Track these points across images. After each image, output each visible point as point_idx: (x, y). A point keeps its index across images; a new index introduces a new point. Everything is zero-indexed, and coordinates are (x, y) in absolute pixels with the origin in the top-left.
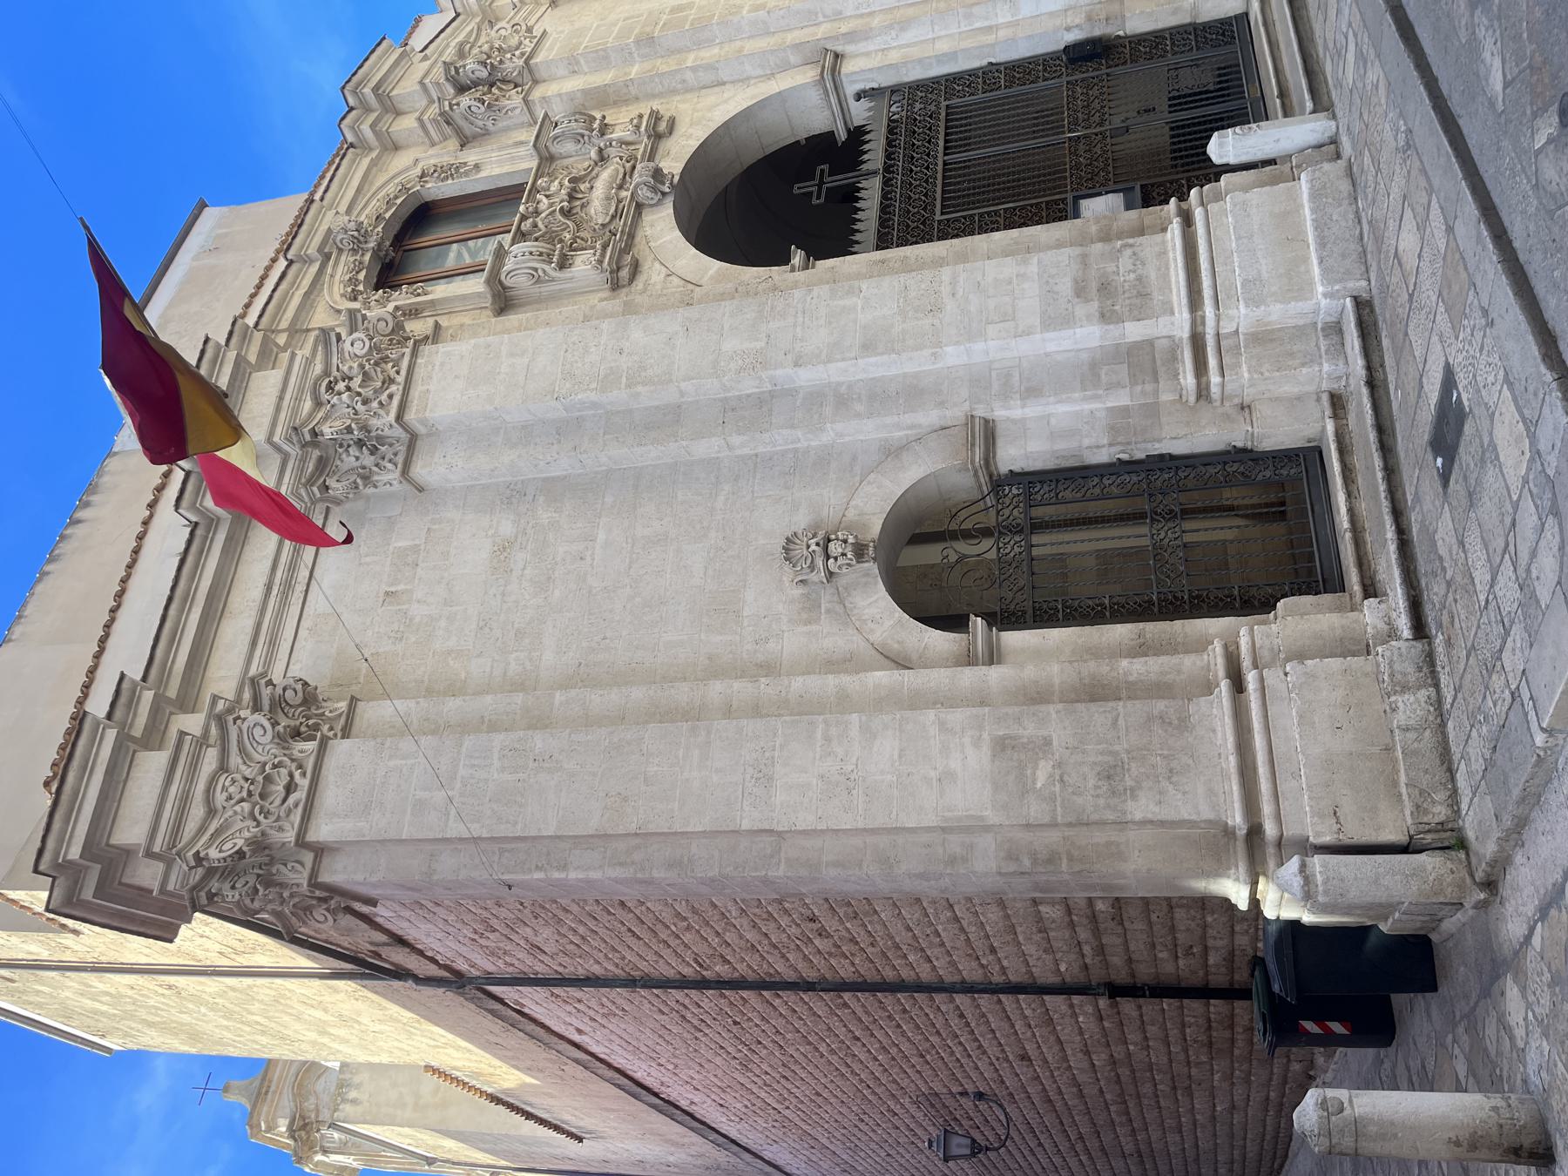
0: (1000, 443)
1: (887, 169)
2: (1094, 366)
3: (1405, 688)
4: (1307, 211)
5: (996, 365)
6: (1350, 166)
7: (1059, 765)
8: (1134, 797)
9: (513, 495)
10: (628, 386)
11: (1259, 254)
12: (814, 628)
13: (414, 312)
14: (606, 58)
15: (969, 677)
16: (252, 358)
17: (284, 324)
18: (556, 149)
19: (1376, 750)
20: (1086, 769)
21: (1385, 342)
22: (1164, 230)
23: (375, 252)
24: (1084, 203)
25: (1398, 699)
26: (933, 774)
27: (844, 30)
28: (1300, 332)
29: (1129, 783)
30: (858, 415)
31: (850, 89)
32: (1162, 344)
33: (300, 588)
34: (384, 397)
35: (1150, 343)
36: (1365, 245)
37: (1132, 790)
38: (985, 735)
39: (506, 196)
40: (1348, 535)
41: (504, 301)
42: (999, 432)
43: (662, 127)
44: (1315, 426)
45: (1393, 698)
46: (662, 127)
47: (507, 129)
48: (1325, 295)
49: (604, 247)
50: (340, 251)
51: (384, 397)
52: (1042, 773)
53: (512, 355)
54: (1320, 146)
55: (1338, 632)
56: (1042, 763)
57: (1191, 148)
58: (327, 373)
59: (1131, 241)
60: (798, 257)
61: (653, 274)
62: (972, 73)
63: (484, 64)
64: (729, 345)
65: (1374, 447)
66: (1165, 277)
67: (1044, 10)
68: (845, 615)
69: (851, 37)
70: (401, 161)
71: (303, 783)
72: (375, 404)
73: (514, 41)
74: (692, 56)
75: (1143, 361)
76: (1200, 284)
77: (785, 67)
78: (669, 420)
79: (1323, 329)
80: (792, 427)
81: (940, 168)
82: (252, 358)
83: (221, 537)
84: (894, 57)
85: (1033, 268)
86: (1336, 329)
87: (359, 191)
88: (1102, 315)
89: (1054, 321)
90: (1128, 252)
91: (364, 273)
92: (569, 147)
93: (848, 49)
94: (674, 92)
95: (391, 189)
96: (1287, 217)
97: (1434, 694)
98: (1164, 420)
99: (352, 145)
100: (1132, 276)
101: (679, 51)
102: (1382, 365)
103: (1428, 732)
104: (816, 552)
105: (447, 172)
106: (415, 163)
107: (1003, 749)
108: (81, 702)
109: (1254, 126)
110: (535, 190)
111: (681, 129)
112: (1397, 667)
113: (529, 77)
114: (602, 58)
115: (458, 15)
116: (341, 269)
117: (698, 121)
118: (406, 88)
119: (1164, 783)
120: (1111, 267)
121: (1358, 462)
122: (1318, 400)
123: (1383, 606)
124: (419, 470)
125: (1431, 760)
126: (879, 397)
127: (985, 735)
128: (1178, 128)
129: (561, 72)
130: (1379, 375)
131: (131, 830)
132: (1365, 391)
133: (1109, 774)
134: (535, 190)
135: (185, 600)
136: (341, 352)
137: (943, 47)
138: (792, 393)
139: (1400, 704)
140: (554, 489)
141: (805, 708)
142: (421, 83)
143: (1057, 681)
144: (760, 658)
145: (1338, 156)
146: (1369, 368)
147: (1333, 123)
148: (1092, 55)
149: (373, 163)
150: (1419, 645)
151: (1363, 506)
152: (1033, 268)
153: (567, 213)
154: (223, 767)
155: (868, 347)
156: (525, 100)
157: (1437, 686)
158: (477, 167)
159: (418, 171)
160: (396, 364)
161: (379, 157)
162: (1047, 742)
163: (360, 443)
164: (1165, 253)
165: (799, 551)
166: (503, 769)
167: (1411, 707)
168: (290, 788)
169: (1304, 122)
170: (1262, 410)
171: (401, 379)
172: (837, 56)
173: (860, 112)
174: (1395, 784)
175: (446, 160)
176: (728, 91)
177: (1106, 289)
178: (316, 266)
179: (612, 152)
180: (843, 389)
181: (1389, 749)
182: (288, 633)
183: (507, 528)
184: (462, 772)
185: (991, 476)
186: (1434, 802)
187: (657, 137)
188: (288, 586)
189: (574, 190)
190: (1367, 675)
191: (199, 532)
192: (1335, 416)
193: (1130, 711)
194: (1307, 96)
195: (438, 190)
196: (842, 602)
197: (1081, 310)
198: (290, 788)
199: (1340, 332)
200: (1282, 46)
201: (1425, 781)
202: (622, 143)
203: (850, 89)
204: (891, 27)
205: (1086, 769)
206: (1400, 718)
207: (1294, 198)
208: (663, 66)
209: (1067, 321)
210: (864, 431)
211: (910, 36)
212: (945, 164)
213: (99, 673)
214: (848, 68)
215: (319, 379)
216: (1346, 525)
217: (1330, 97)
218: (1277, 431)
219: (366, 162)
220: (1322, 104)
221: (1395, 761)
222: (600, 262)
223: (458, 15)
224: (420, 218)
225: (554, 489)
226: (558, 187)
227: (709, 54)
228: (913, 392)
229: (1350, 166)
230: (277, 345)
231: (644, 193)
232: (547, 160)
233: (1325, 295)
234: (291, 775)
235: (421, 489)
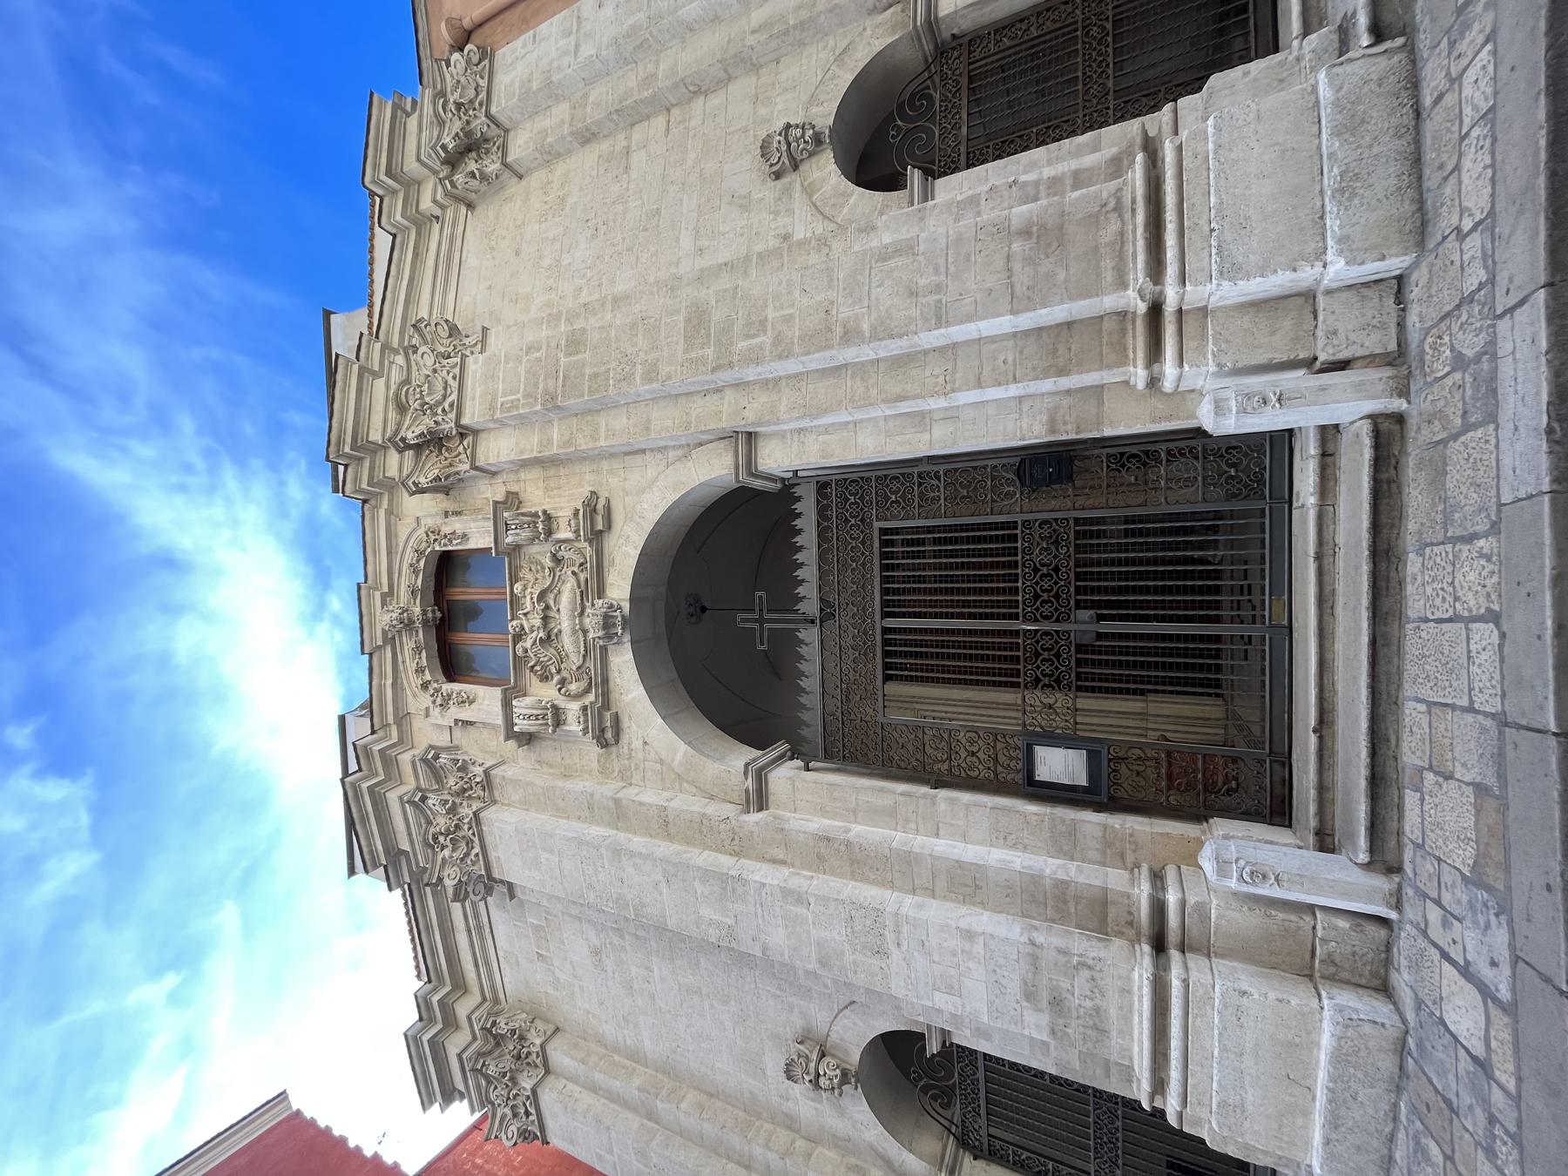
11: (1247, 1079)
33: (487, 930)
50: (399, 632)
66: (1127, 1020)
68: (842, 1113)
76: (1167, 1048)
87: (389, 553)
91: (424, 654)
95: (410, 556)
104: (810, 1060)
115: (394, 236)
120: (1065, 984)
135: (427, 929)
182: (493, 957)
185: (944, 1042)
187: (597, 537)
188: (480, 928)
198: (527, 1114)
223: (394, 236)
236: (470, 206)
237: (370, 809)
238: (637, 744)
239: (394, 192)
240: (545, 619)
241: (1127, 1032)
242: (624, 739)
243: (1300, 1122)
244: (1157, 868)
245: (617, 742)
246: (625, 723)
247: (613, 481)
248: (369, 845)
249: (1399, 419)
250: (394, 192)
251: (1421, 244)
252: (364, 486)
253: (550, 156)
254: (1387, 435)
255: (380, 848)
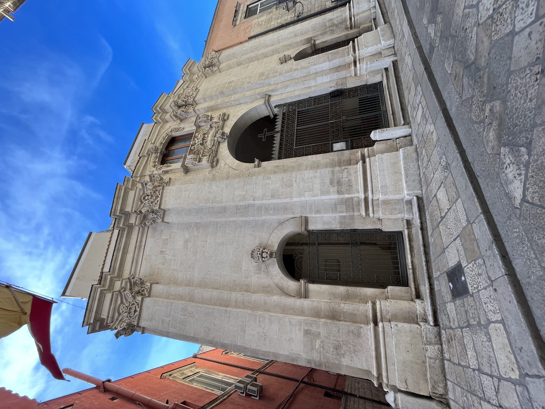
0: (309, 224)
1: (282, 131)
2: (336, 205)
3: (430, 344)
4: (402, 163)
5: (308, 202)
6: (416, 148)
7: (322, 342)
8: (344, 357)
9: (187, 226)
10: (212, 203)
11: (386, 177)
12: (259, 275)
13: (166, 172)
14: (213, 97)
15: (300, 302)
16: (130, 187)
17: (139, 175)
18: (200, 124)
19: (420, 361)
20: (330, 345)
21: (428, 217)
22: (357, 163)
23: (161, 153)
24: (334, 145)
25: (428, 347)
26: (287, 338)
27: (270, 89)
28: (399, 201)
29: (343, 352)
30: (271, 214)
31: (273, 105)
32: (355, 199)
33: (143, 247)
34: (156, 201)
35: (352, 198)
36: (422, 181)
37: (343, 355)
38: (302, 328)
39: (188, 137)
40: (411, 271)
41: (186, 170)
42: (309, 220)
43: (226, 118)
44: (400, 227)
45: (426, 346)
46: (226, 118)
47: (191, 117)
48: (407, 195)
49: (209, 156)
51: (156, 201)
52: (318, 344)
53: (185, 191)
54: (405, 137)
55: (408, 309)
56: (317, 340)
57: (367, 127)
58: (144, 194)
59: (347, 167)
60: (257, 161)
61: (222, 163)
62: (304, 100)
63: (183, 101)
64: (237, 193)
65: (422, 253)
66: (357, 180)
67: (324, 81)
68: (267, 273)
69: (273, 91)
70: (167, 126)
71: (138, 310)
72: (154, 204)
73: (191, 94)
74: (233, 97)
75: (350, 205)
77: (257, 99)
78: (224, 210)
79: (406, 202)
80: (254, 216)
81: (295, 131)
82: (130, 187)
83: (126, 232)
84: (284, 96)
85: (318, 174)
86: (410, 202)
87: (157, 135)
88: (338, 192)
89: (323, 193)
90: (346, 171)
92: (203, 124)
93: (272, 94)
94: (229, 106)
95: (164, 135)
96: (395, 164)
97: (440, 348)
98: (356, 221)
99: (156, 123)
100: (347, 179)
101: (230, 95)
102: (426, 222)
103: (438, 361)
104: (260, 254)
105: (177, 130)
106: (171, 127)
107: (307, 334)
108: (102, 269)
109: (385, 129)
110: (195, 137)
111: (230, 118)
112: (428, 335)
113: (194, 103)
114: (211, 98)
116: (152, 158)
117: (236, 115)
118: (167, 107)
119: (353, 354)
121: (414, 244)
122: (403, 221)
123: (423, 304)
124: (166, 220)
125: (439, 371)
126: (277, 209)
127: (302, 328)
128: (363, 120)
129: (202, 101)
130: (424, 225)
131: (104, 315)
132: (420, 232)
133: (337, 348)
134: (195, 137)
136: (147, 188)
137: (297, 93)
138: (254, 205)
139: (429, 349)
140: (198, 226)
141: (254, 307)
142: (170, 106)
143: (323, 308)
144: (246, 283)
145: (412, 145)
146: (421, 223)
147: (410, 130)
148: (338, 94)
149: (161, 127)
150: (436, 328)
151: (416, 261)
152: (318, 174)
153: (202, 144)
154: (122, 302)
155: (273, 196)
156: (194, 110)
157: (441, 344)
158: (183, 128)
159: (170, 130)
160: (159, 191)
161: (163, 125)
162: (319, 334)
163: (153, 212)
164: (357, 172)
165: (255, 255)
166: (181, 315)
167: (432, 350)
168: (135, 311)
169: (401, 129)
170: (385, 222)
171: (160, 196)
172: (269, 96)
173: (276, 110)
174: (426, 375)
175: (177, 126)
176: (242, 106)
177: (339, 183)
178: (146, 158)
179: (214, 125)
180: (267, 206)
181: (424, 362)
183: (187, 236)
184: (172, 313)
186: (439, 386)
187: (224, 121)
188: (140, 247)
189: (204, 137)
190: (418, 334)
191: (120, 232)
192: (408, 228)
193: (343, 325)
194: (402, 119)
195: (175, 134)
196: (267, 268)
197: (332, 190)
198: (135, 311)
199: (411, 204)
200: (393, 96)
201: (436, 378)
202: (216, 123)
203: (273, 105)
204: (283, 88)
205: (330, 345)
206: (428, 354)
207: (398, 157)
208: (226, 99)
209: (328, 193)
210: (274, 218)
211: (288, 90)
212: (297, 130)
213: (106, 261)
214: (272, 99)
215: (142, 196)
216: (410, 267)
217: (409, 119)
218: (388, 227)
219: (159, 127)
220: (407, 123)
221: (426, 367)
222: (208, 161)
224: (172, 141)
225: (198, 226)
226: (200, 136)
227: (237, 96)
228: (285, 208)
229: (416, 148)
230: (137, 181)
231: (220, 140)
232: (198, 127)
233: (407, 195)
234: (135, 307)
235: (168, 223)
236: (206, 77)
237: (122, 194)
238: (223, 165)
239: (188, 74)
240: (203, 139)
241: (357, 184)
242: (219, 165)
243: (400, 183)
244: (367, 216)
245: (216, 166)
246: (220, 161)
247: (232, 111)
248: (116, 207)
249: (396, 61)
250: (188, 74)
251: (394, 37)
252: (158, 118)
253: (230, 67)
254: (395, 63)
255: (119, 208)
